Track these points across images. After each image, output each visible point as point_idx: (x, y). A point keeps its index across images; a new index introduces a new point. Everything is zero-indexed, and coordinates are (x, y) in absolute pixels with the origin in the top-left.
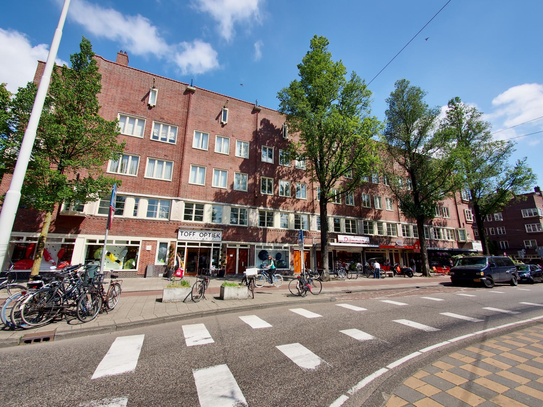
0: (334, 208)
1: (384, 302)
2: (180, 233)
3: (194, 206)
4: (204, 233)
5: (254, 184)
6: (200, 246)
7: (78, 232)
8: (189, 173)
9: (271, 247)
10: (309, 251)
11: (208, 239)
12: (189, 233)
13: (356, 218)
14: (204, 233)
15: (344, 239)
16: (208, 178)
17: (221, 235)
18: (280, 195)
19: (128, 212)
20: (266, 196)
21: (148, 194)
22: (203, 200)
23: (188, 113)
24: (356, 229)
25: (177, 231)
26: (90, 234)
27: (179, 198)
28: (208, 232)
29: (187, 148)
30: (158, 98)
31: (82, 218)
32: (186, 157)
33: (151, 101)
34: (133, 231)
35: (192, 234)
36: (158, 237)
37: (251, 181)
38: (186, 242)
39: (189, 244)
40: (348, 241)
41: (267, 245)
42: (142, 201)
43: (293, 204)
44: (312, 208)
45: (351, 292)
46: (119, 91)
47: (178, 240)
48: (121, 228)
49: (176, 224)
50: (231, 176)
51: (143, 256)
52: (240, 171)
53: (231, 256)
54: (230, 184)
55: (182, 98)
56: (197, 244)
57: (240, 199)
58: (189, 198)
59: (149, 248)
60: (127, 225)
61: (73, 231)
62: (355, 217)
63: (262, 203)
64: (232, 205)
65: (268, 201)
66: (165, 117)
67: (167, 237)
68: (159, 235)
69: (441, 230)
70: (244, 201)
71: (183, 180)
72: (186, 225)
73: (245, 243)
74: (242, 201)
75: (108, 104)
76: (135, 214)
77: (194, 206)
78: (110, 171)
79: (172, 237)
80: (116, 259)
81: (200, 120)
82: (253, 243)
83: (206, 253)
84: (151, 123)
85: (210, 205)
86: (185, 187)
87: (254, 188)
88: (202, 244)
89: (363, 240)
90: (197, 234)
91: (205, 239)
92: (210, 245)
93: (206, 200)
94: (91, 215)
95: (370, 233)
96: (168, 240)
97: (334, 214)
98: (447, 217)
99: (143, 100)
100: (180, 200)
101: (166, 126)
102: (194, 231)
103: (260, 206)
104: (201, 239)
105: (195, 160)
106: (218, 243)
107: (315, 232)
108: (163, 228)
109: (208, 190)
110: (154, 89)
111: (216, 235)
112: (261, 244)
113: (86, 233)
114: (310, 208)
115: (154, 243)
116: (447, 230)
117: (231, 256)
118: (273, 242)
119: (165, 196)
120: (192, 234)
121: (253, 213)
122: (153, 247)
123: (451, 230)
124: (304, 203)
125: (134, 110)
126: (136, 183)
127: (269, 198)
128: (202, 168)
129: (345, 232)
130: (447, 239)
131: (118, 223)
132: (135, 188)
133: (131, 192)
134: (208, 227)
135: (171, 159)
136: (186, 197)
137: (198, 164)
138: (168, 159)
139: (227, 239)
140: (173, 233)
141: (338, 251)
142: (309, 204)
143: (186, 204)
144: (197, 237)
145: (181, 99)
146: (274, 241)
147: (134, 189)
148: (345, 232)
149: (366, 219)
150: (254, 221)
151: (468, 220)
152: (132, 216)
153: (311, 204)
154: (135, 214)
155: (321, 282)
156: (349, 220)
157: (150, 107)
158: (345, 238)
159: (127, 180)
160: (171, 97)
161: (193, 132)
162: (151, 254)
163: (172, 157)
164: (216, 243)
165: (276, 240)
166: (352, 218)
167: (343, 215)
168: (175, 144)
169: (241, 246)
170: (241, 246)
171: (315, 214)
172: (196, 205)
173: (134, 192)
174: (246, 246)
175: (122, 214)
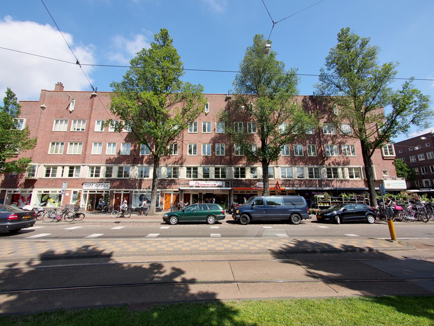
0: (202, 159)
1: (114, 230)
2: (84, 185)
3: (192, 169)
4: (98, 185)
5: (134, 150)
6: (96, 193)
7: (33, 188)
8: (92, 148)
9: (145, 192)
10: (179, 194)
11: (101, 188)
12: (89, 185)
13: (225, 166)
14: (98, 185)
15: (195, 184)
16: (104, 149)
17: (109, 186)
18: (308, 156)
19: (58, 175)
20: (143, 157)
21: (68, 163)
22: (100, 164)
23: (91, 110)
24: (320, 175)
25: (83, 184)
26: (39, 188)
27: (278, 166)
28: (101, 184)
29: (90, 132)
30: (75, 105)
31: (35, 181)
32: (89, 138)
33: (71, 108)
34: (59, 185)
35: (91, 185)
36: (72, 188)
37: (132, 148)
38: (104, 191)
39: (90, 192)
40: (199, 186)
41: (142, 190)
42: (65, 168)
43: (165, 160)
44: (181, 162)
45: (119, 223)
46: (55, 107)
47: (83, 189)
48: (53, 184)
49: (83, 180)
50: (119, 146)
51: (64, 199)
52: (125, 142)
53: (118, 198)
54: (117, 152)
55: (89, 101)
56: (95, 192)
57: (124, 161)
58: (91, 164)
59: (67, 194)
60: (57, 182)
61: (31, 187)
62: (224, 164)
63: (140, 162)
64: (118, 165)
65: (144, 160)
66: (79, 116)
67: (77, 188)
68: (73, 187)
69: (340, 170)
70: (127, 162)
71: (87, 153)
72: (88, 180)
73: (125, 190)
74: (125, 162)
75: (49, 115)
76: (62, 176)
77: (192, 169)
78: (73, 153)
79: (80, 188)
80: (53, 201)
81: (100, 113)
82: (131, 190)
83: (99, 196)
84: (71, 121)
85: (104, 166)
86: (89, 157)
87: (135, 152)
88: (98, 192)
89: (216, 183)
90: (94, 185)
91: (99, 188)
92: (103, 192)
93: (101, 164)
94: (40, 178)
95: (241, 177)
96: (78, 190)
97: (202, 164)
98: (352, 155)
99: (67, 108)
100: (85, 165)
101: (79, 122)
102: (92, 184)
103: (138, 164)
104: (97, 188)
105: (96, 140)
106: (108, 190)
107: (183, 180)
108: (76, 182)
109: (103, 157)
110: (73, 100)
111: (106, 185)
112: (137, 190)
113: (37, 188)
114: (180, 162)
115: (70, 191)
116: (350, 169)
117: (118, 198)
118: (147, 189)
119: (77, 163)
120: (91, 185)
121: (132, 170)
122: (69, 194)
123: (356, 169)
124: (176, 158)
125: (62, 116)
126: (62, 158)
127: (146, 158)
128: (100, 144)
129: (214, 178)
130: (348, 178)
131: (52, 181)
132: (61, 161)
133: (59, 163)
134: (101, 181)
135: (81, 141)
136: (89, 163)
137: (97, 141)
138: (79, 141)
139: (114, 188)
140: (81, 185)
141: (204, 193)
142: (180, 159)
143: (215, 168)
144: (94, 187)
145: (88, 102)
146: (148, 188)
147: (61, 162)
148: (214, 178)
149: (237, 166)
150: (132, 175)
151: (385, 156)
152: (60, 177)
153: (180, 159)
154: (62, 176)
155: (395, 224)
156: (331, 169)
157: (71, 112)
158: (196, 183)
159: (57, 157)
160: (82, 103)
161: (95, 122)
162: (68, 198)
163: (82, 140)
164: (106, 190)
165: (149, 187)
166: (221, 166)
167: (211, 164)
168: (84, 131)
169: (124, 192)
170: (124, 192)
171: (184, 165)
172: (96, 167)
173: (61, 163)
174: (128, 192)
175: (55, 176)
